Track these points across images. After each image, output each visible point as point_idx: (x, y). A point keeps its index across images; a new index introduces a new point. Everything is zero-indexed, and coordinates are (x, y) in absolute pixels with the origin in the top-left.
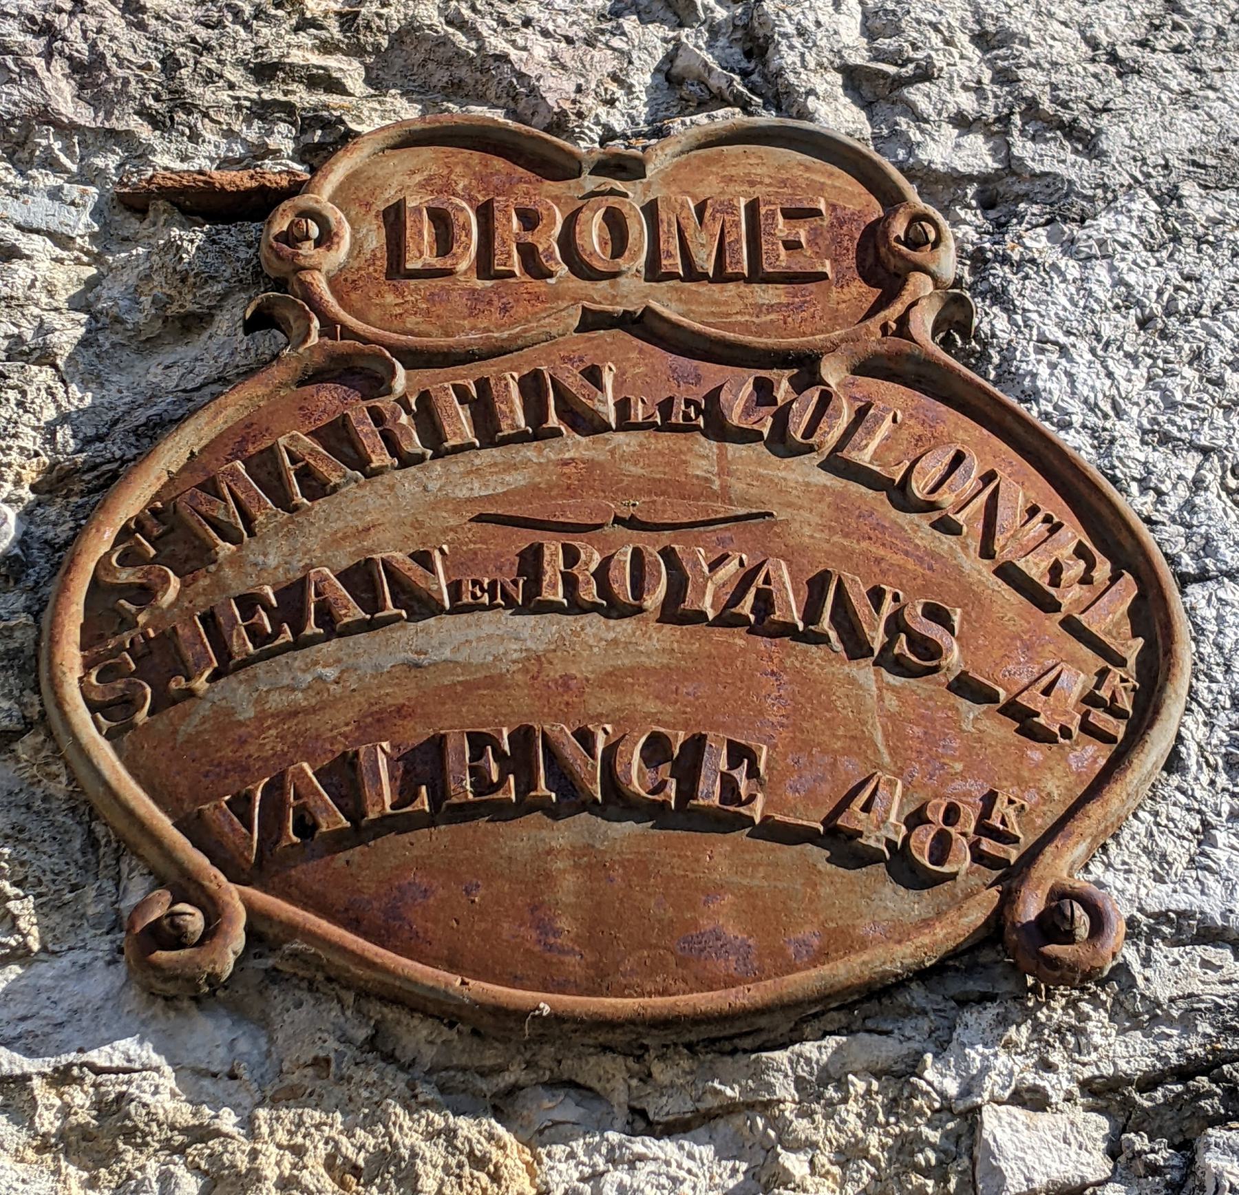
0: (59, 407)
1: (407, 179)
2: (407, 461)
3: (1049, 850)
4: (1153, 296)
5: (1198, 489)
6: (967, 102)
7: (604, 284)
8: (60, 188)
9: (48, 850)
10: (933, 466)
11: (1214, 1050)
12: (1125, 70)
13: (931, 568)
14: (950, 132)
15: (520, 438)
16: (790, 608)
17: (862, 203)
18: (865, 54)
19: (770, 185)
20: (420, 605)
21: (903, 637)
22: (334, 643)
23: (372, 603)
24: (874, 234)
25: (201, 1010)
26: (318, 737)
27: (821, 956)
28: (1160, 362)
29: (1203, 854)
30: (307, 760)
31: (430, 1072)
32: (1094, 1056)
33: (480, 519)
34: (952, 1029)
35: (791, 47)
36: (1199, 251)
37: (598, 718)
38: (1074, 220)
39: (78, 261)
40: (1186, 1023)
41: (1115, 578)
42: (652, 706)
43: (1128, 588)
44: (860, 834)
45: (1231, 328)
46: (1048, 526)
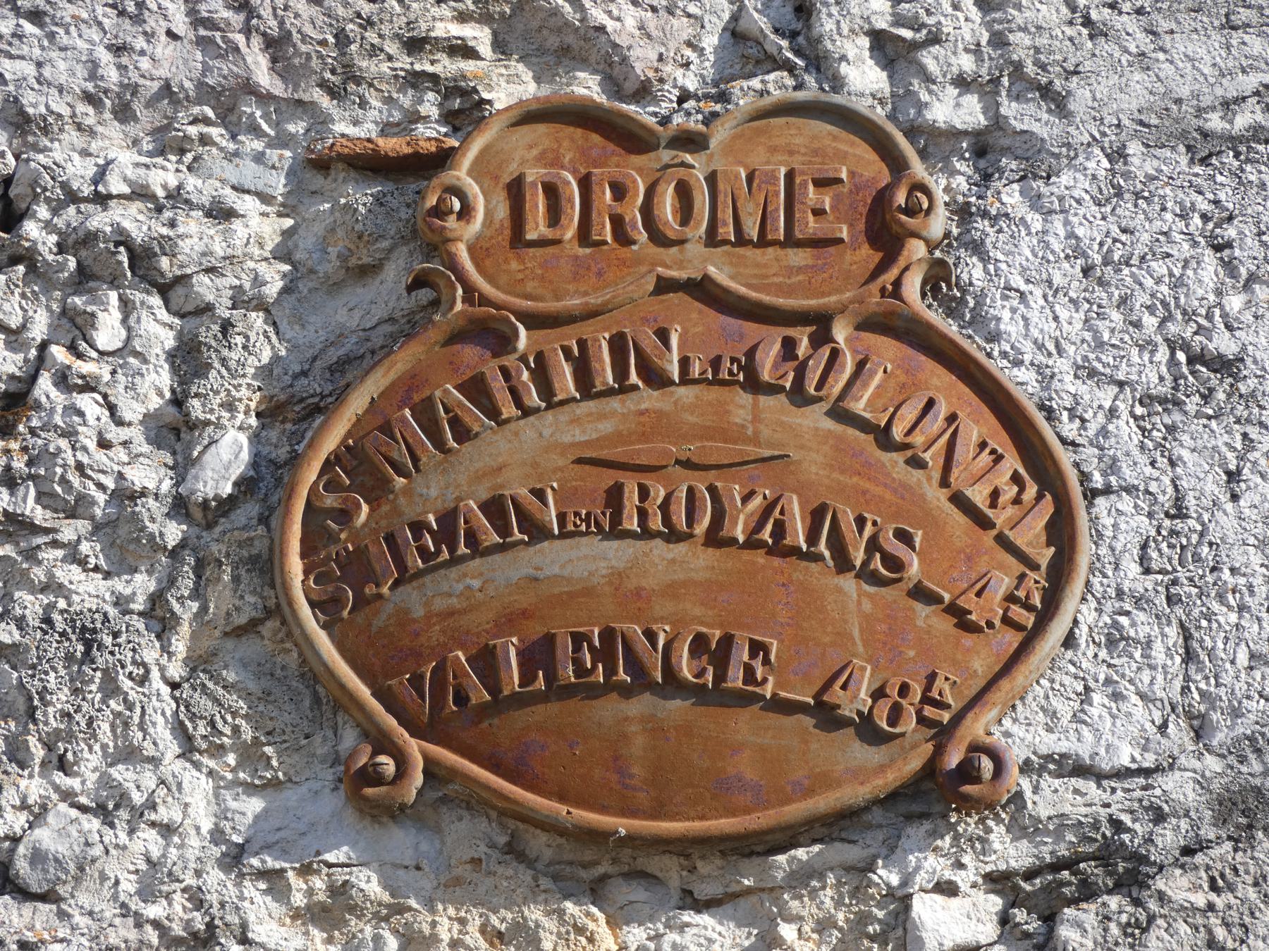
0: (273, 348)
1: (527, 154)
2: (527, 412)
3: (970, 715)
4: (1096, 247)
5: (1112, 416)
6: (967, 63)
7: (674, 250)
8: (263, 154)
9: (288, 709)
10: (909, 413)
11: (1076, 852)
12: (1096, 31)
13: (903, 498)
14: (952, 91)
15: (610, 392)
16: (798, 535)
17: (875, 170)
18: (889, 18)
19: (805, 154)
20: (536, 532)
21: (878, 556)
22: (478, 561)
23: (504, 531)
24: (882, 198)
25: (395, 822)
26: (468, 632)
27: (809, 792)
28: (1095, 308)
29: (1083, 711)
30: (462, 649)
31: (548, 865)
32: (994, 857)
33: (580, 461)
34: (899, 837)
35: (830, 15)
36: (1136, 206)
37: (663, 620)
38: (1041, 177)
39: (280, 215)
40: (1058, 834)
41: (1040, 497)
42: (698, 611)
43: (1047, 508)
44: (839, 707)
45: (1152, 277)
46: (993, 457)
